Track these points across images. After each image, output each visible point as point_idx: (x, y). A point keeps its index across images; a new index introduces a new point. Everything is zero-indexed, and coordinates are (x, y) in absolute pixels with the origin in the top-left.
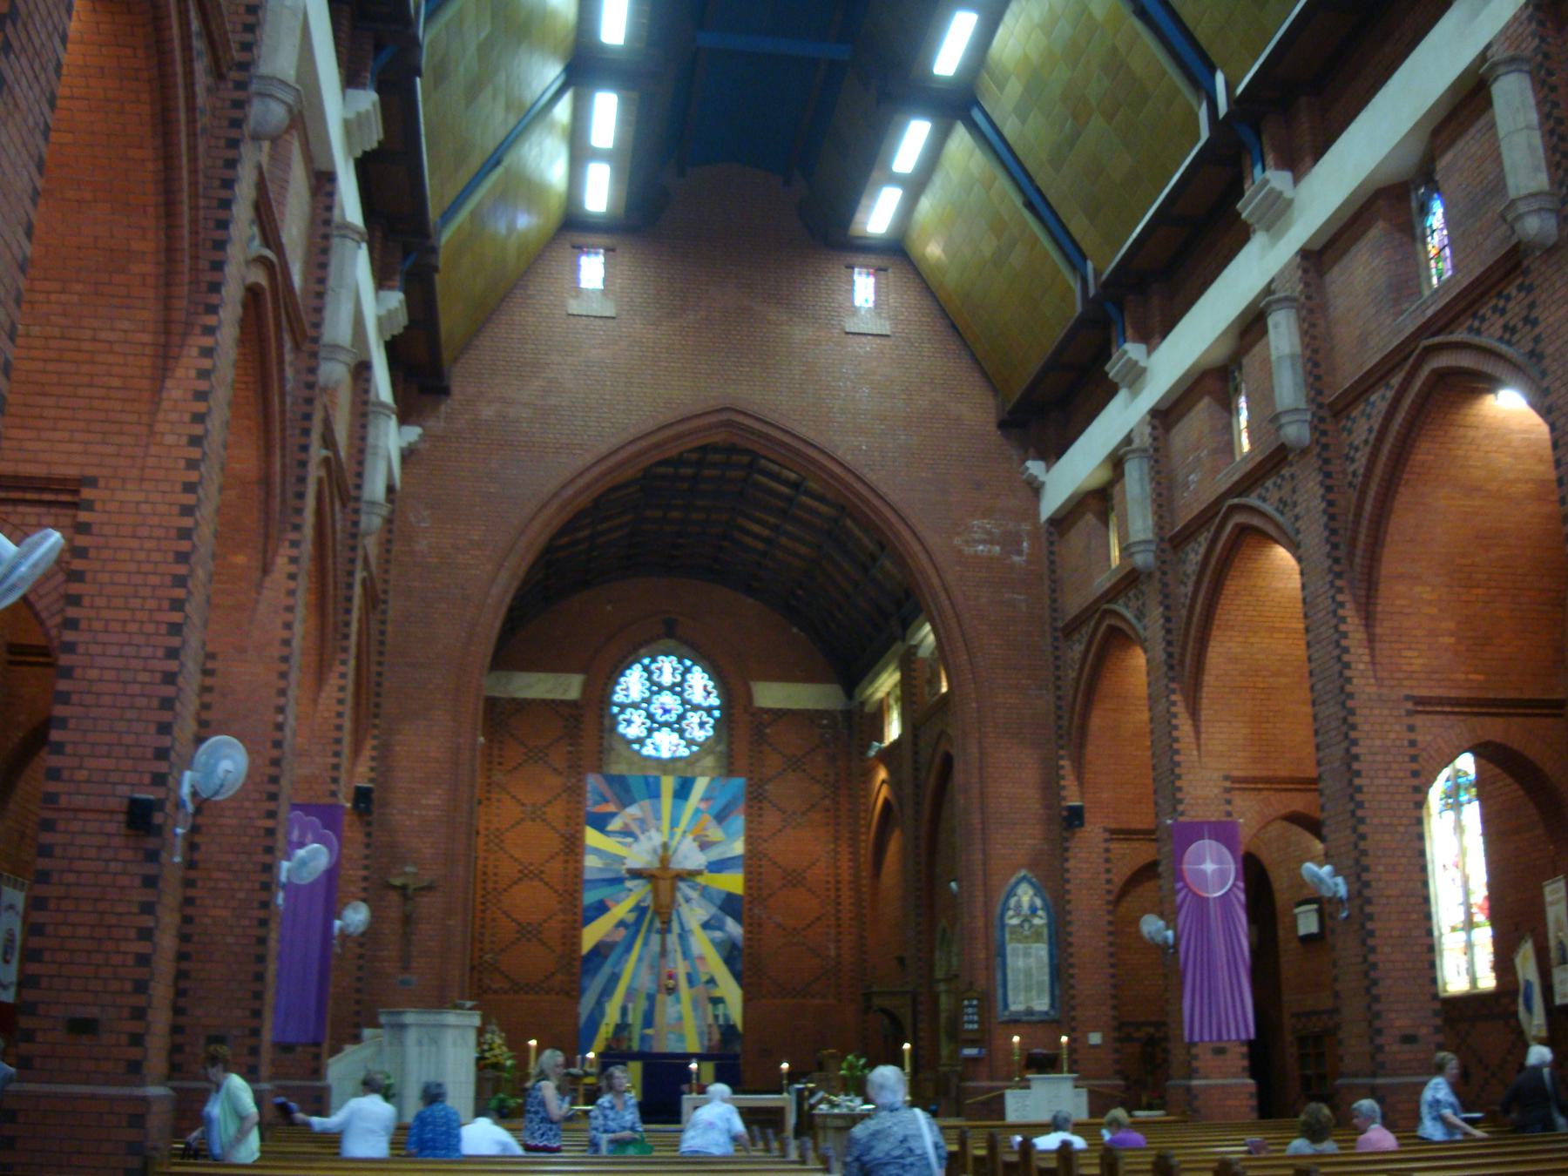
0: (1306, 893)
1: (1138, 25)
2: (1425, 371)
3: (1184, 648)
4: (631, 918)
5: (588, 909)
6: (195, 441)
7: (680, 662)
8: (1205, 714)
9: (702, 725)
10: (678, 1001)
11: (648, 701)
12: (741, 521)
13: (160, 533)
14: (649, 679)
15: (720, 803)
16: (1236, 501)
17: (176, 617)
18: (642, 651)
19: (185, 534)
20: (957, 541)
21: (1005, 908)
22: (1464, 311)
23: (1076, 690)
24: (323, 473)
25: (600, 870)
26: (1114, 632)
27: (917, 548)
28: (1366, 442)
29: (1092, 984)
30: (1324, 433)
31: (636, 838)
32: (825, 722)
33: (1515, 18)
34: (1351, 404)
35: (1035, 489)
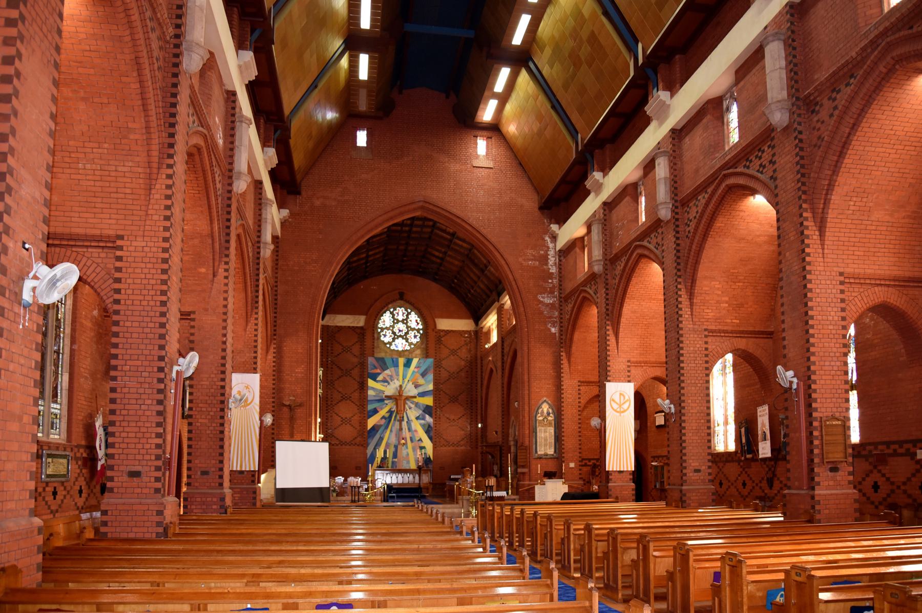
0: (659, 409)
1: (604, 20)
2: (724, 185)
3: (613, 307)
4: (387, 415)
6: (167, 218)
8: (621, 335)
9: (415, 337)
10: (407, 448)
11: (393, 327)
12: (429, 250)
14: (393, 317)
16: (638, 243)
17: (164, 298)
18: (390, 306)
19: (165, 261)
20: (520, 259)
21: (537, 413)
22: (743, 157)
23: (569, 323)
24: (241, 231)
26: (585, 298)
27: (503, 262)
28: (695, 217)
29: (570, 443)
30: (677, 213)
33: (780, 12)
34: (689, 200)
35: (554, 238)
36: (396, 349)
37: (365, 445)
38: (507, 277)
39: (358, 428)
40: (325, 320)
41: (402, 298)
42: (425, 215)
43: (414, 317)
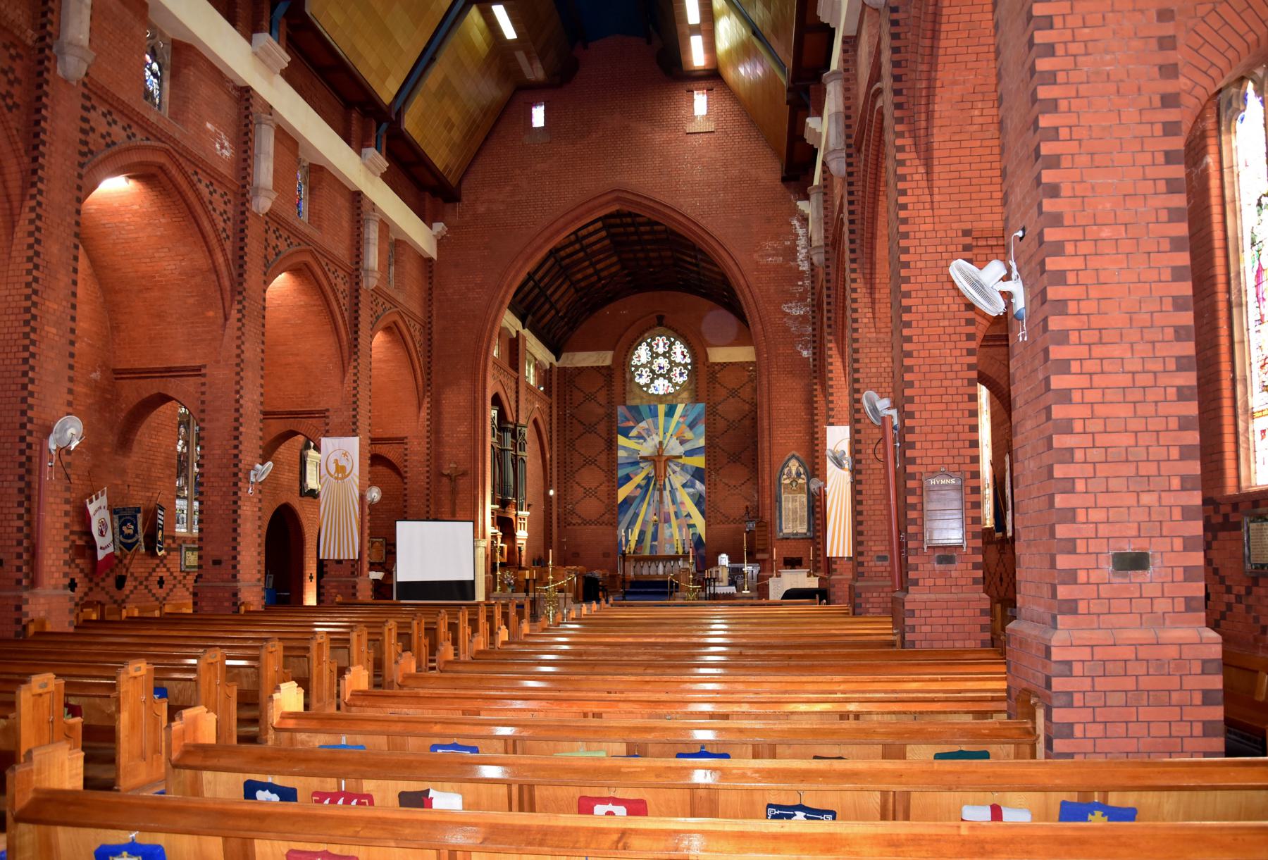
4: (643, 483)
5: (621, 478)
7: (668, 339)
9: (681, 374)
13: (16, 311)
15: (691, 418)
18: (646, 335)
20: (756, 256)
21: (782, 473)
25: (626, 458)
27: (731, 263)
31: (645, 440)
36: (656, 393)
37: (614, 525)
38: (739, 285)
39: (606, 501)
40: (561, 361)
41: (661, 323)
42: (626, 208)
43: (679, 348)
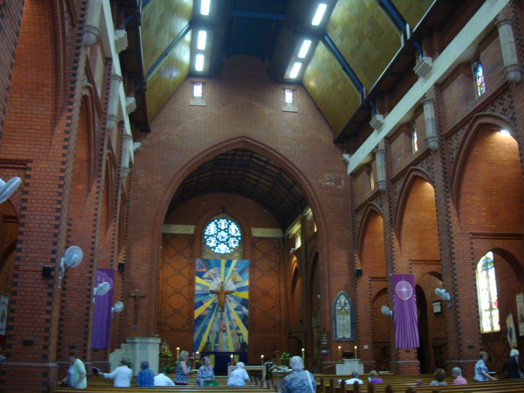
0: (436, 298)
1: (380, 8)
2: (476, 124)
3: (396, 217)
4: (211, 307)
5: (196, 304)
6: (65, 147)
7: (227, 221)
8: (403, 239)
9: (235, 242)
10: (227, 334)
11: (217, 234)
12: (248, 174)
13: (53, 178)
14: (217, 227)
15: (241, 268)
16: (413, 167)
17: (59, 206)
18: (215, 218)
19: (62, 178)
20: (320, 181)
21: (336, 304)
22: (489, 104)
23: (360, 231)
24: (108, 158)
25: (201, 291)
26: (372, 211)
27: (306, 183)
28: (457, 148)
29: (365, 329)
30: (442, 145)
31: (213, 280)
32: (276, 241)
33: (506, 6)
34: (451, 135)
35: (346, 163)
